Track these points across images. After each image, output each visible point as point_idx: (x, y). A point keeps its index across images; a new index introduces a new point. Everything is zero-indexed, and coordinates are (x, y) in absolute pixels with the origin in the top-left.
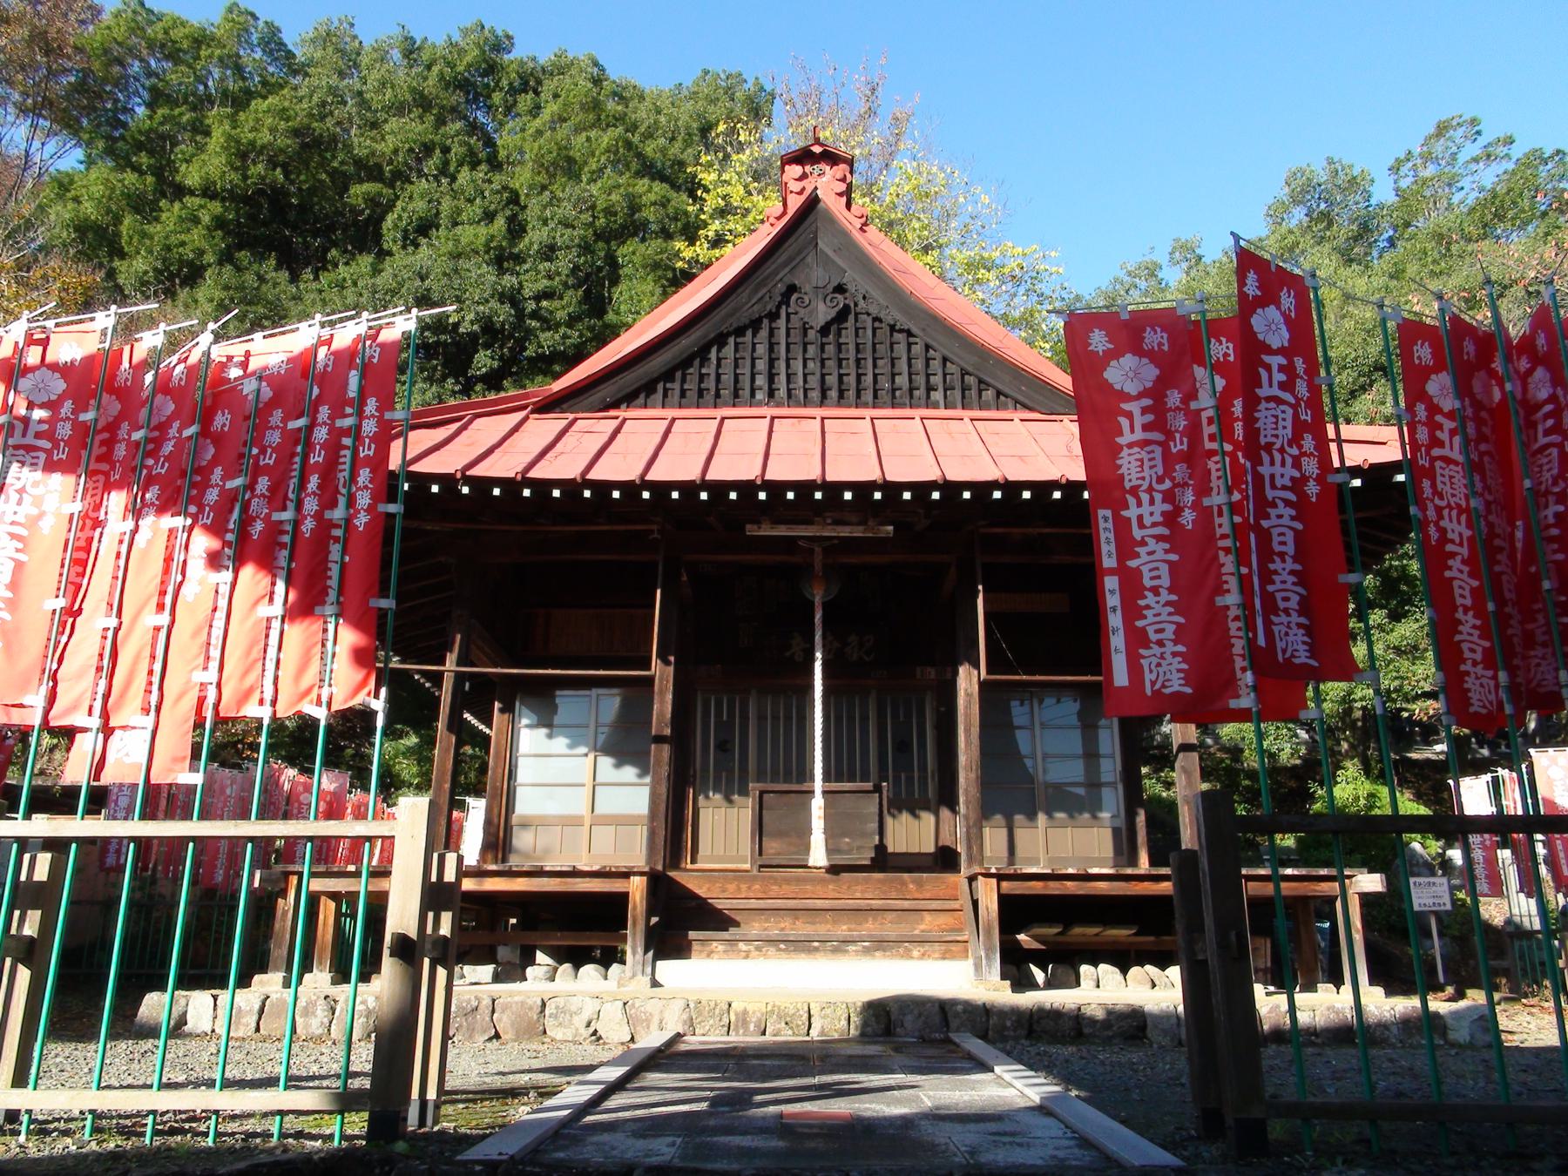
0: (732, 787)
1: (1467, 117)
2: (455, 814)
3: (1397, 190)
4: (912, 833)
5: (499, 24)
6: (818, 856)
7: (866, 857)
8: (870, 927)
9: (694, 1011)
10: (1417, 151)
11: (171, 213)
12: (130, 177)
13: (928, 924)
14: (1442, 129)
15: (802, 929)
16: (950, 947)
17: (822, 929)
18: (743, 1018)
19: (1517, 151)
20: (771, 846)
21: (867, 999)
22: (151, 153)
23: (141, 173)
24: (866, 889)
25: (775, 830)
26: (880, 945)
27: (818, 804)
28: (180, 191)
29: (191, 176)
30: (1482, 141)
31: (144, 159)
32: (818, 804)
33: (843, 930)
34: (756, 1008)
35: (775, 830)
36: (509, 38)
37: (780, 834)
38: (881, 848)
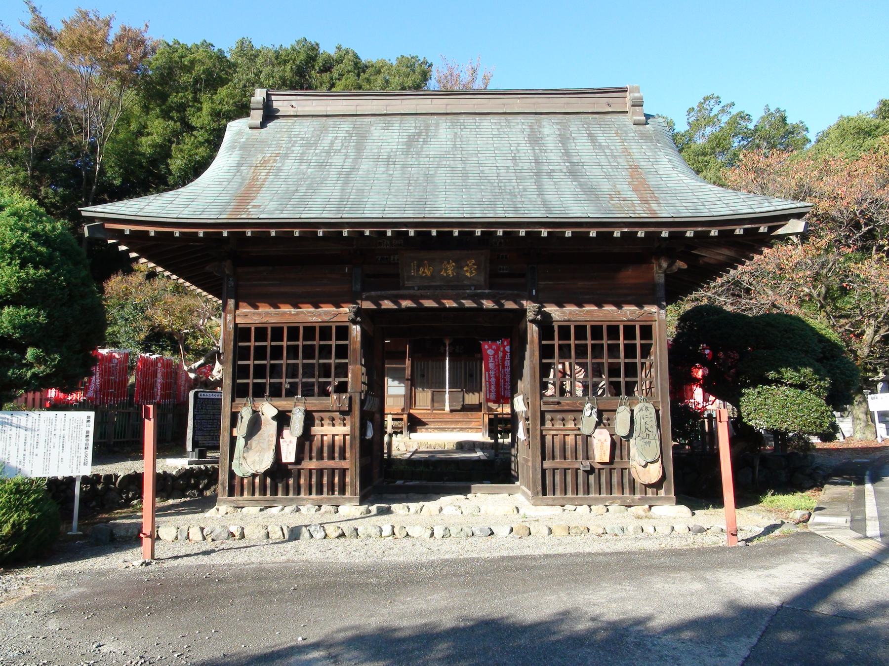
0: (424, 386)
1: (715, 95)
2: (619, 501)
3: (689, 123)
4: (472, 399)
5: (312, 40)
6: (447, 409)
7: (459, 407)
8: (459, 425)
9: (420, 444)
10: (696, 108)
11: (188, 140)
12: (171, 123)
13: (473, 424)
14: (706, 99)
15: (444, 426)
16: (477, 430)
17: (448, 426)
18: (430, 445)
19: (734, 111)
20: (436, 405)
21: (733, 595)
22: (178, 111)
23: (176, 122)
24: (458, 416)
25: (437, 401)
26: (462, 429)
27: (447, 396)
28: (193, 128)
29: (194, 122)
30: (721, 105)
31: (174, 114)
32: (447, 396)
33: (453, 426)
34: (433, 443)
35: (437, 401)
36: (317, 45)
37: (438, 402)
38: (463, 405)
